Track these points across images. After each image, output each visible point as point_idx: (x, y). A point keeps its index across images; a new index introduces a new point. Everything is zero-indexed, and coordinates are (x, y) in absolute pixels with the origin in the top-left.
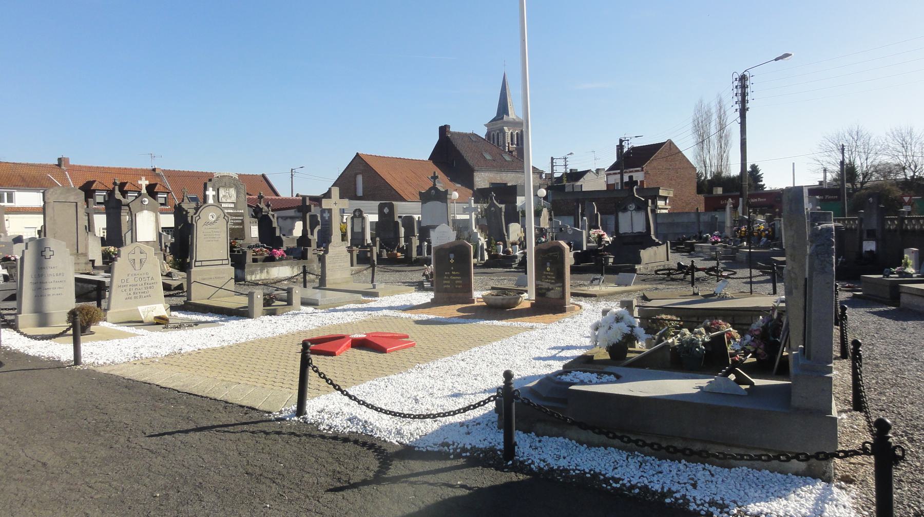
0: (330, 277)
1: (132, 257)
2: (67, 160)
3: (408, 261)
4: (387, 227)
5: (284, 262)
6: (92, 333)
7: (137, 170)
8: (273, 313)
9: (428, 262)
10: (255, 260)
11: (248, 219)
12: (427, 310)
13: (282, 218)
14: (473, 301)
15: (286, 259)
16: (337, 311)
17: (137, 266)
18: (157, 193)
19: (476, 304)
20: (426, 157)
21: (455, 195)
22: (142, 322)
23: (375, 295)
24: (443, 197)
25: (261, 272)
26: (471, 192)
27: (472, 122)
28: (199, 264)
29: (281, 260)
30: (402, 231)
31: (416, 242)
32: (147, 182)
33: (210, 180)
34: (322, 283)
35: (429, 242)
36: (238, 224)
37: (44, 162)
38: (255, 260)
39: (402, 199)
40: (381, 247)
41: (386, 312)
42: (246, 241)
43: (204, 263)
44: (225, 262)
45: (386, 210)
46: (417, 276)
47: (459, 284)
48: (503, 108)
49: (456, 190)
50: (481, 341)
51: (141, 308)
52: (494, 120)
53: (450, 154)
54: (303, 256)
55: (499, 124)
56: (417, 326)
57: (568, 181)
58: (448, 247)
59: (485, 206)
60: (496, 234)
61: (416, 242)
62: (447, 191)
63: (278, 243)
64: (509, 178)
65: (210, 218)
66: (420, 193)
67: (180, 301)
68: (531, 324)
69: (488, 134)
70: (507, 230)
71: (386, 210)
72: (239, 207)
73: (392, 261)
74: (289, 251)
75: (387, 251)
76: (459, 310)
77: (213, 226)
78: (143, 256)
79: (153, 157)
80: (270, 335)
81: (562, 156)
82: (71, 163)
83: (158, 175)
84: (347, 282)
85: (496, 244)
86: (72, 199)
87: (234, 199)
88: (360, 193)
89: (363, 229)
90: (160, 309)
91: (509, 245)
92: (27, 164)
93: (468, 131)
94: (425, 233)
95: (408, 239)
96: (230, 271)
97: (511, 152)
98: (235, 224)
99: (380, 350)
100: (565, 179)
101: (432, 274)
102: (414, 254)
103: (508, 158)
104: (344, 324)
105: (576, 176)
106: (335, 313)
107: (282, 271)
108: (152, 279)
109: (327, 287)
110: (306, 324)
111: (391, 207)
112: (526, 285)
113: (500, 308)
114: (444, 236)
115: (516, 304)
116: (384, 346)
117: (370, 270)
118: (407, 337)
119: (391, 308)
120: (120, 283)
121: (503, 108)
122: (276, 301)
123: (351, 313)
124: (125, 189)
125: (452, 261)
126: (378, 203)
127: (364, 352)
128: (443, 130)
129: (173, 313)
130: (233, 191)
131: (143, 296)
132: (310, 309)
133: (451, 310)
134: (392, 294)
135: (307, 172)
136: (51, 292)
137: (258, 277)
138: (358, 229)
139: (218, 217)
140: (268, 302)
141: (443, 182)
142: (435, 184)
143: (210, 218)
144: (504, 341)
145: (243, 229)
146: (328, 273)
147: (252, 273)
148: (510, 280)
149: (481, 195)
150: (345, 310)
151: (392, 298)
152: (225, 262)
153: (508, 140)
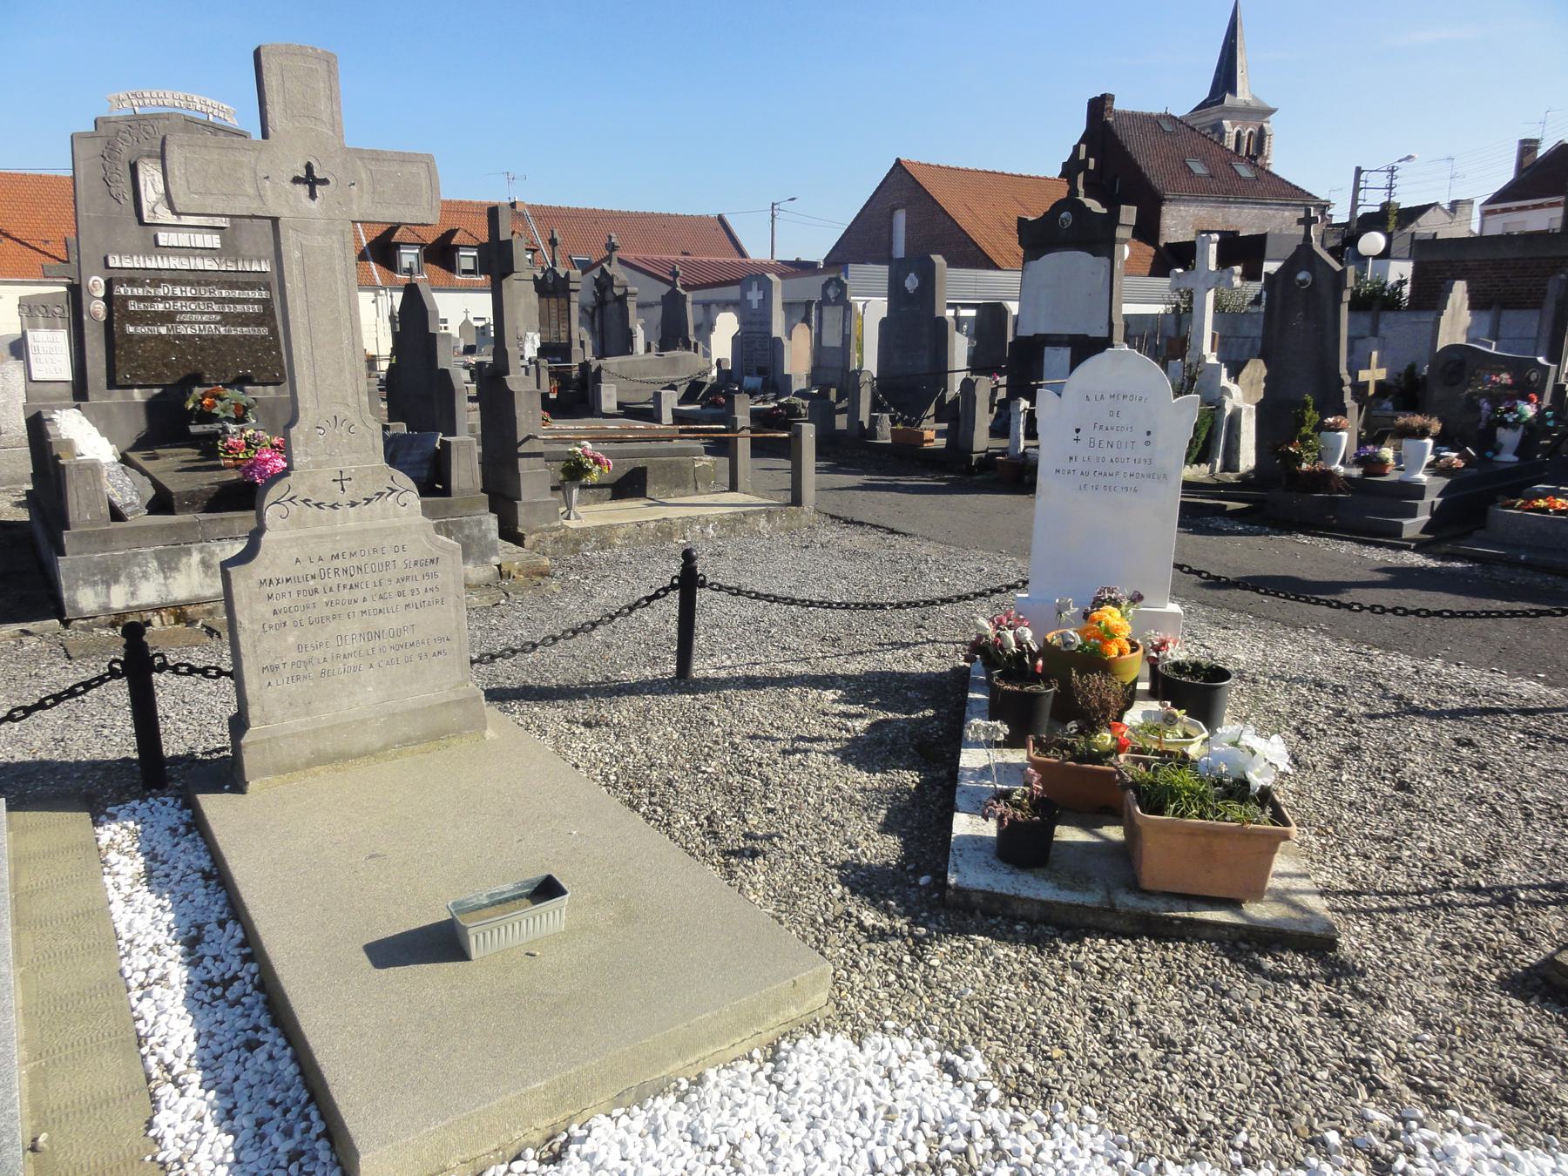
25: (168, 565)
27: (1166, 87)
36: (245, 320)
48: (1226, 78)
55: (1213, 113)
58: (1267, 930)
71: (911, 283)
79: (510, 178)
83: (520, 215)
98: (227, 319)
102: (982, 440)
121: (1226, 78)
124: (455, 241)
128: (1098, 106)
147: (109, 575)
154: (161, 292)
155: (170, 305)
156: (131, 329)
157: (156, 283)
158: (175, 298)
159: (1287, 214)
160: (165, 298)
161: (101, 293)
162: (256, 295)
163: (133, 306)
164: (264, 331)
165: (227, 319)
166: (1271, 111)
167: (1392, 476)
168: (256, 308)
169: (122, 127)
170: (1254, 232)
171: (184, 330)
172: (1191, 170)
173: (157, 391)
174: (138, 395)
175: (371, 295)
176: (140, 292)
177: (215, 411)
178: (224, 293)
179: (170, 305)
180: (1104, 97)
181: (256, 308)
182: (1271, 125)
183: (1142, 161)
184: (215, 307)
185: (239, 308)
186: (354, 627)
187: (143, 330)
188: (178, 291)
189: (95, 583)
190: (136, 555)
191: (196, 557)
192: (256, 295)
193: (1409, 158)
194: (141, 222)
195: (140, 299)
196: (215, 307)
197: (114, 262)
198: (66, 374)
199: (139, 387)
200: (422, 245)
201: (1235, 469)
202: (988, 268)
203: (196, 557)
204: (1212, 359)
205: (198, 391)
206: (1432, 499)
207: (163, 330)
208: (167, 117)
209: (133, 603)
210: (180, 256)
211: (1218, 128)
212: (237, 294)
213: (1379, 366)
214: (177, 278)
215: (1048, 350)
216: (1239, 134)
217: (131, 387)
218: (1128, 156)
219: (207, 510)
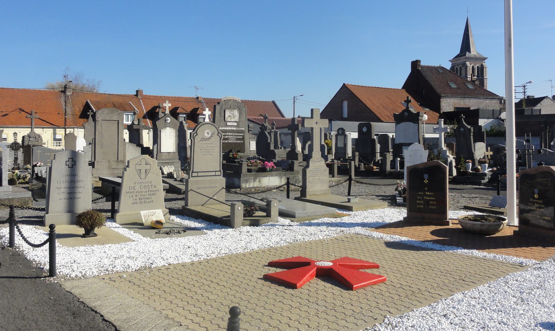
0: (310, 189)
1: (139, 167)
3: (382, 174)
4: (365, 143)
5: (274, 173)
6: (95, 235)
7: (186, 98)
8: (255, 223)
9: (400, 176)
10: (249, 171)
11: (247, 136)
12: (399, 230)
13: (284, 134)
14: (448, 223)
15: (276, 170)
16: (310, 225)
17: (143, 175)
18: (178, 114)
19: (451, 226)
20: (400, 87)
21: (426, 117)
22: (142, 224)
23: (349, 209)
24: (415, 118)
25: (254, 181)
26: (438, 115)
27: (439, 55)
29: (271, 170)
30: (378, 146)
31: (390, 157)
33: (219, 103)
34: (303, 197)
35: (402, 158)
37: (127, 93)
38: (249, 171)
39: (379, 120)
40: (360, 161)
41: (358, 229)
42: (245, 154)
43: (200, 174)
45: (365, 129)
46: (390, 191)
47: (433, 205)
48: (466, 46)
49: (425, 113)
50: (466, 281)
51: (143, 213)
52: (458, 56)
53: (422, 85)
54: (291, 168)
55: (462, 59)
56: (388, 249)
57: (527, 106)
58: (422, 167)
59: (456, 126)
60: (464, 153)
61: (390, 157)
62: (418, 113)
63: (272, 155)
64: (472, 104)
65: (206, 134)
66: (395, 115)
67: (179, 205)
68: (522, 260)
69: (452, 68)
70: (474, 146)
71: (365, 129)
73: (368, 174)
74: (277, 164)
75: (365, 164)
76: (433, 233)
77: (208, 142)
78: (148, 167)
79: (197, 89)
80: (241, 251)
81: (521, 84)
82: (144, 93)
83: (200, 102)
84: (325, 194)
85: (465, 162)
86: (115, 118)
87: (237, 119)
88: (345, 115)
89: (345, 145)
90: (158, 214)
91: (477, 163)
92: (117, 95)
93: (437, 65)
94: (398, 149)
95: (382, 154)
96: (222, 181)
97: (474, 81)
98: (237, 139)
99: (347, 286)
100: (524, 104)
101: (404, 190)
102: (388, 168)
103: (470, 86)
104: (316, 242)
105: (533, 101)
106: (309, 228)
107: (273, 180)
109: (308, 198)
110: (278, 239)
111: (369, 127)
112: (503, 205)
113: (479, 235)
114: (415, 155)
115: (497, 231)
116: (351, 281)
117: (346, 184)
118: (377, 267)
119: (363, 225)
121: (466, 46)
122: (256, 213)
123: (324, 228)
124: (178, 111)
125: (426, 181)
126: (359, 123)
127: (328, 285)
128: (415, 64)
129: (173, 217)
130: (236, 112)
131: (146, 201)
132: (287, 221)
133: (424, 233)
134: (366, 208)
135: (304, 97)
137: (251, 185)
138: (340, 145)
140: (248, 213)
141: (414, 107)
142: (408, 107)
143: (206, 134)
144: (493, 284)
145: (244, 144)
146: (308, 185)
147: (247, 181)
148: (481, 198)
149: (449, 117)
150: (318, 225)
151: (366, 213)
153: (470, 72)
157: (226, 132)
159: (487, 101)
165: (237, 139)
166: (485, 59)
167: (481, 172)
168: (242, 137)
170: (476, 108)
172: (450, 86)
175: (147, 131)
180: (417, 61)
182: (486, 64)
183: (432, 83)
186: (317, 178)
193: (530, 82)
201: (452, 175)
202: (379, 122)
204: (445, 149)
205: (231, 153)
206: (489, 176)
211: (464, 65)
213: (491, 151)
215: (403, 147)
216: (473, 67)
218: (427, 81)
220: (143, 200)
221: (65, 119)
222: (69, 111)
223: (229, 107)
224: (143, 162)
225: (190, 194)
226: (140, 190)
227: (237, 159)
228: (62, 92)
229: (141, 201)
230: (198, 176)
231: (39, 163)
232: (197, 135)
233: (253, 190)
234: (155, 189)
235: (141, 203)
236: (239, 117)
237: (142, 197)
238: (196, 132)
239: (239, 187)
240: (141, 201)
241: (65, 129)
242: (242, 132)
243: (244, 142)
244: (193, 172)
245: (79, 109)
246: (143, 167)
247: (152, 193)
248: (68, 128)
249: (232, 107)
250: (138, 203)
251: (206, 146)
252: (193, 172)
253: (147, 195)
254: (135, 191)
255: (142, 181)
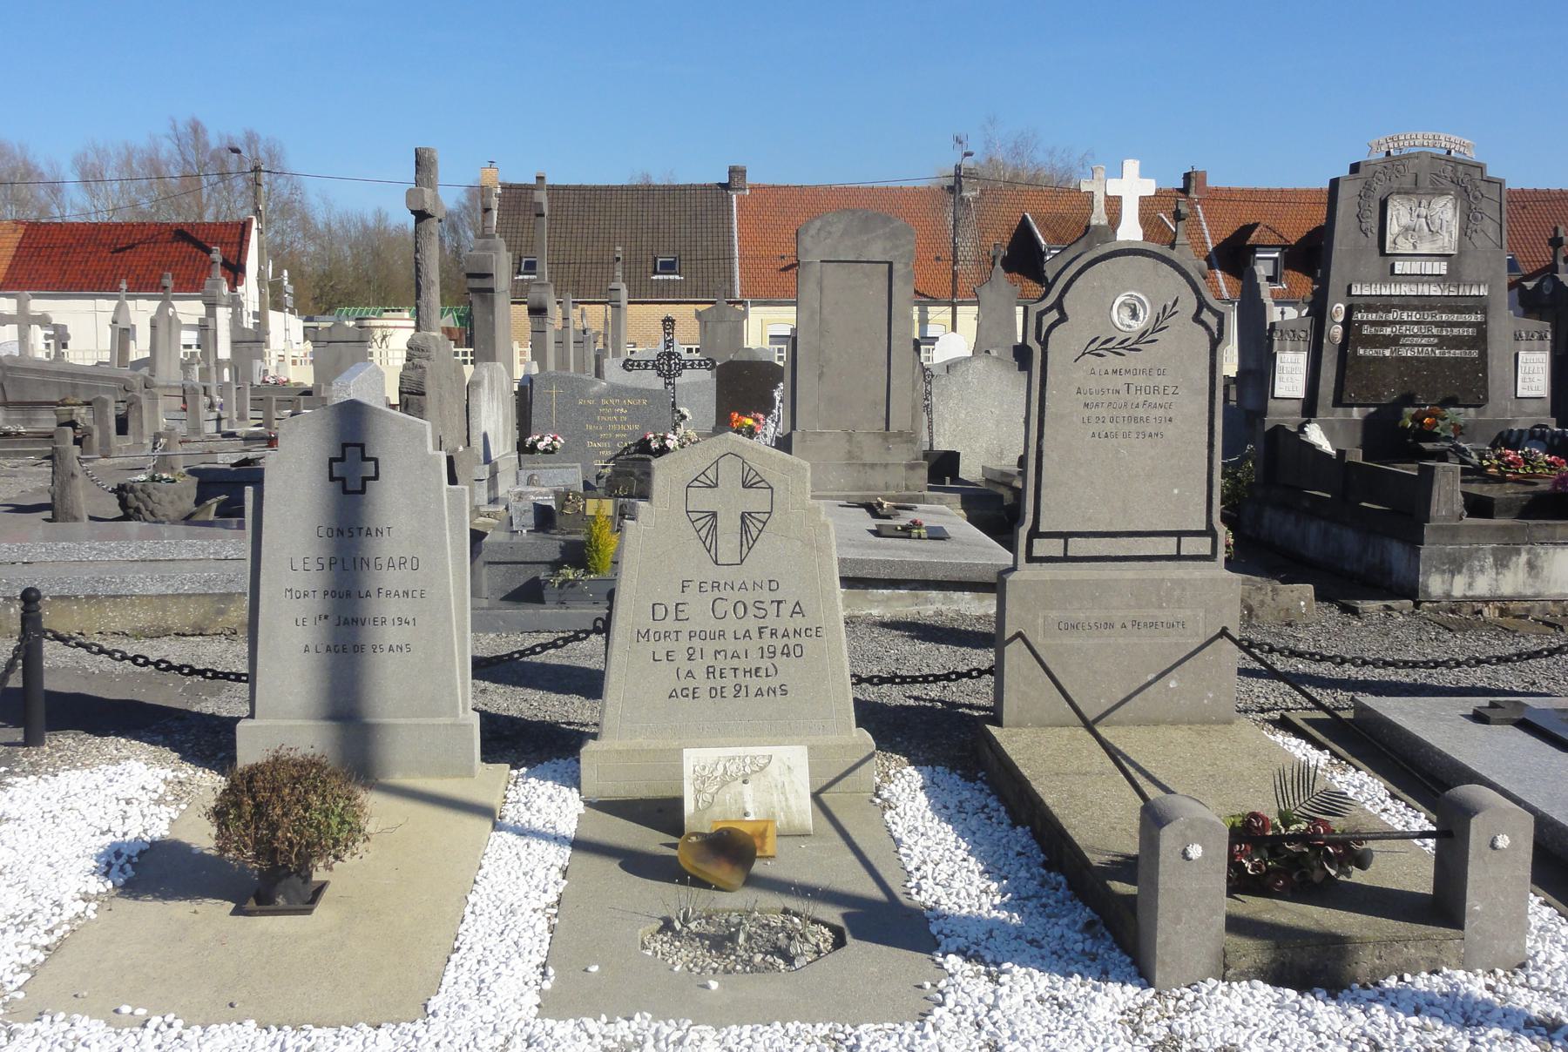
1: (704, 500)
2: (1203, 176)
11: (1505, 321)
25: (1501, 563)
28: (1052, 547)
32: (1149, 188)
36: (1457, 342)
38: (1478, 507)
42: (1489, 413)
43: (1078, 547)
44: (1191, 546)
51: (695, 760)
65: (1120, 317)
72: (1468, 271)
77: (1131, 360)
78: (756, 501)
82: (1211, 183)
86: (876, 251)
87: (1448, 241)
98: (1443, 342)
108: (797, 609)
120: (646, 622)
130: (1446, 211)
131: (738, 684)
136: (390, 635)
139: (1164, 316)
143: (1120, 317)
145: (1482, 363)
147: (1455, 565)
152: (1191, 546)
154: (1391, 317)
155: (1396, 329)
156: (1361, 352)
157: (1388, 308)
158: (1402, 323)
160: (1393, 323)
161: (1340, 319)
162: (1473, 318)
163: (1367, 330)
164: (1475, 353)
165: (1443, 342)
168: (1471, 331)
169: (1379, 168)
171: (1406, 353)
173: (1372, 410)
174: (1356, 413)
176: (1373, 317)
177: (1437, 430)
178: (1444, 317)
179: (1396, 329)
181: (1471, 331)
184: (1435, 331)
185: (1456, 331)
187: (1371, 352)
188: (1405, 317)
189: (1444, 572)
190: (1477, 550)
191: (1524, 557)
192: (1473, 318)
194: (1383, 253)
195: (1373, 323)
196: (1435, 331)
197: (1356, 291)
198: (1300, 392)
199: (1359, 406)
200: (1283, 247)
203: (1524, 557)
205: (1410, 411)
207: (1387, 353)
208: (1417, 156)
209: (1470, 593)
210: (1410, 283)
212: (1455, 318)
214: (1406, 303)
217: (1352, 406)
219: (1520, 516)
220: (729, 682)
221: (955, 275)
222: (967, 248)
223: (1407, 183)
224: (730, 474)
225: (1015, 655)
226: (713, 625)
227: (1434, 437)
228: (951, 189)
229: (718, 683)
230: (1066, 559)
231: (548, 440)
232: (1063, 318)
233: (1490, 613)
234: (799, 622)
235: (717, 693)
236: (1464, 231)
237: (720, 663)
238: (1058, 305)
239: (1410, 591)
240: (718, 683)
241: (954, 306)
242: (1479, 304)
243: (1484, 354)
244: (1035, 533)
245: (1000, 239)
246: (730, 502)
247: (779, 643)
248: (962, 303)
249: (1425, 182)
250: (703, 692)
251: (1120, 382)
252: (1035, 533)
253: (755, 654)
254: (686, 628)
255: (723, 575)
